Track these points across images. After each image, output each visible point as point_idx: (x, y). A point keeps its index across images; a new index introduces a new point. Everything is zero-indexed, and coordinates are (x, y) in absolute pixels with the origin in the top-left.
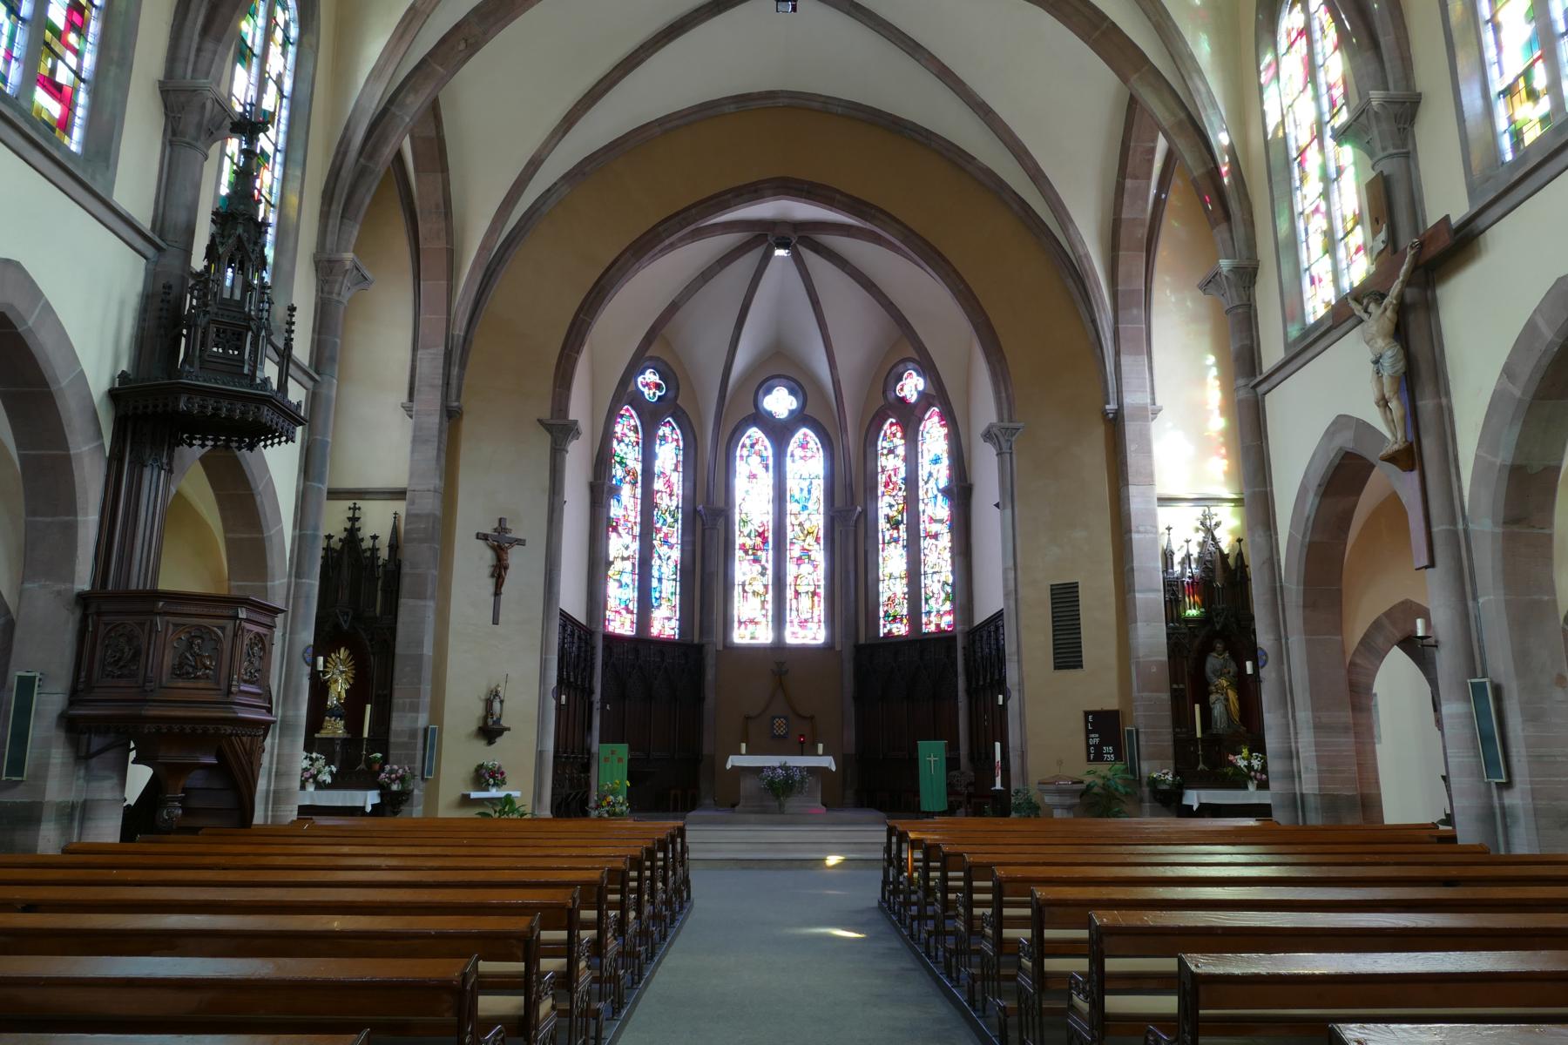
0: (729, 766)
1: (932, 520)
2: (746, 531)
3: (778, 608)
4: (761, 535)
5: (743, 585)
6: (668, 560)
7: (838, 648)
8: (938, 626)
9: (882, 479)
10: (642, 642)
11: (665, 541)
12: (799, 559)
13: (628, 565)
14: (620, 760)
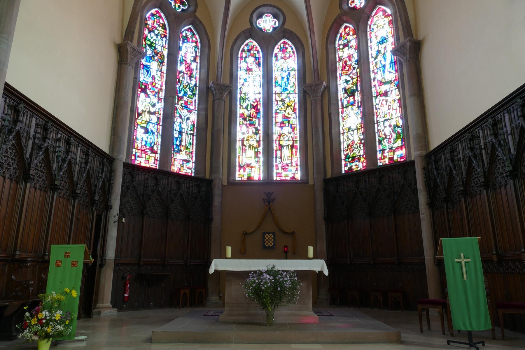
0: (211, 271)
1: (381, 83)
2: (245, 105)
3: (266, 155)
4: (255, 107)
5: (243, 141)
6: (187, 119)
7: (311, 183)
8: (391, 159)
9: (339, 65)
10: (162, 174)
11: (185, 106)
12: (282, 123)
13: (154, 118)
14: (74, 264)
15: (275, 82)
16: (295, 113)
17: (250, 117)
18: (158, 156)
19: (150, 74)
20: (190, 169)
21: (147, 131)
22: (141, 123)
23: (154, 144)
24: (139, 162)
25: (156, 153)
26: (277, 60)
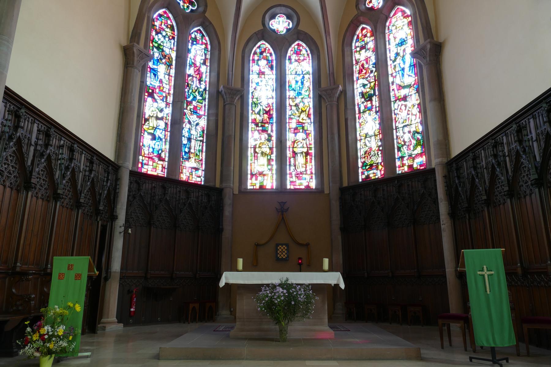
0: (222, 284)
1: (400, 87)
2: (257, 110)
3: (279, 162)
4: (268, 112)
5: (255, 148)
6: (196, 125)
7: (326, 191)
8: (411, 167)
9: (356, 68)
10: (170, 182)
11: (195, 111)
12: (296, 129)
15: (289, 86)
16: (310, 118)
17: (262, 122)
18: (166, 163)
19: (158, 78)
20: (199, 177)
21: (154, 138)
22: (148, 129)
23: (162, 151)
24: (146, 170)
25: (163, 160)
26: (291, 63)
